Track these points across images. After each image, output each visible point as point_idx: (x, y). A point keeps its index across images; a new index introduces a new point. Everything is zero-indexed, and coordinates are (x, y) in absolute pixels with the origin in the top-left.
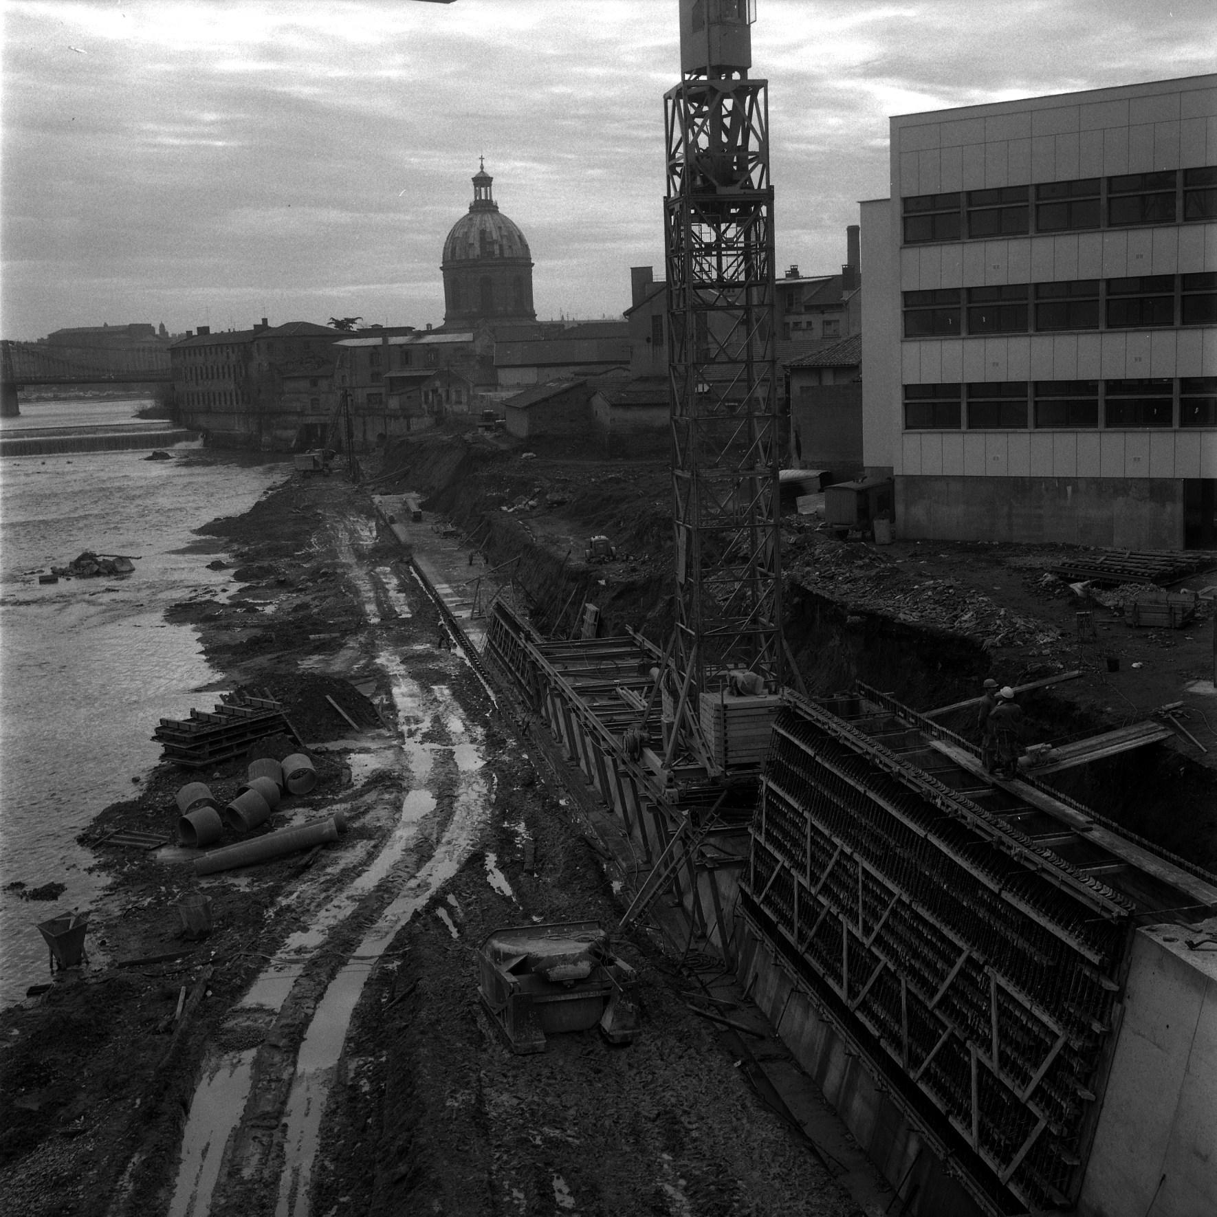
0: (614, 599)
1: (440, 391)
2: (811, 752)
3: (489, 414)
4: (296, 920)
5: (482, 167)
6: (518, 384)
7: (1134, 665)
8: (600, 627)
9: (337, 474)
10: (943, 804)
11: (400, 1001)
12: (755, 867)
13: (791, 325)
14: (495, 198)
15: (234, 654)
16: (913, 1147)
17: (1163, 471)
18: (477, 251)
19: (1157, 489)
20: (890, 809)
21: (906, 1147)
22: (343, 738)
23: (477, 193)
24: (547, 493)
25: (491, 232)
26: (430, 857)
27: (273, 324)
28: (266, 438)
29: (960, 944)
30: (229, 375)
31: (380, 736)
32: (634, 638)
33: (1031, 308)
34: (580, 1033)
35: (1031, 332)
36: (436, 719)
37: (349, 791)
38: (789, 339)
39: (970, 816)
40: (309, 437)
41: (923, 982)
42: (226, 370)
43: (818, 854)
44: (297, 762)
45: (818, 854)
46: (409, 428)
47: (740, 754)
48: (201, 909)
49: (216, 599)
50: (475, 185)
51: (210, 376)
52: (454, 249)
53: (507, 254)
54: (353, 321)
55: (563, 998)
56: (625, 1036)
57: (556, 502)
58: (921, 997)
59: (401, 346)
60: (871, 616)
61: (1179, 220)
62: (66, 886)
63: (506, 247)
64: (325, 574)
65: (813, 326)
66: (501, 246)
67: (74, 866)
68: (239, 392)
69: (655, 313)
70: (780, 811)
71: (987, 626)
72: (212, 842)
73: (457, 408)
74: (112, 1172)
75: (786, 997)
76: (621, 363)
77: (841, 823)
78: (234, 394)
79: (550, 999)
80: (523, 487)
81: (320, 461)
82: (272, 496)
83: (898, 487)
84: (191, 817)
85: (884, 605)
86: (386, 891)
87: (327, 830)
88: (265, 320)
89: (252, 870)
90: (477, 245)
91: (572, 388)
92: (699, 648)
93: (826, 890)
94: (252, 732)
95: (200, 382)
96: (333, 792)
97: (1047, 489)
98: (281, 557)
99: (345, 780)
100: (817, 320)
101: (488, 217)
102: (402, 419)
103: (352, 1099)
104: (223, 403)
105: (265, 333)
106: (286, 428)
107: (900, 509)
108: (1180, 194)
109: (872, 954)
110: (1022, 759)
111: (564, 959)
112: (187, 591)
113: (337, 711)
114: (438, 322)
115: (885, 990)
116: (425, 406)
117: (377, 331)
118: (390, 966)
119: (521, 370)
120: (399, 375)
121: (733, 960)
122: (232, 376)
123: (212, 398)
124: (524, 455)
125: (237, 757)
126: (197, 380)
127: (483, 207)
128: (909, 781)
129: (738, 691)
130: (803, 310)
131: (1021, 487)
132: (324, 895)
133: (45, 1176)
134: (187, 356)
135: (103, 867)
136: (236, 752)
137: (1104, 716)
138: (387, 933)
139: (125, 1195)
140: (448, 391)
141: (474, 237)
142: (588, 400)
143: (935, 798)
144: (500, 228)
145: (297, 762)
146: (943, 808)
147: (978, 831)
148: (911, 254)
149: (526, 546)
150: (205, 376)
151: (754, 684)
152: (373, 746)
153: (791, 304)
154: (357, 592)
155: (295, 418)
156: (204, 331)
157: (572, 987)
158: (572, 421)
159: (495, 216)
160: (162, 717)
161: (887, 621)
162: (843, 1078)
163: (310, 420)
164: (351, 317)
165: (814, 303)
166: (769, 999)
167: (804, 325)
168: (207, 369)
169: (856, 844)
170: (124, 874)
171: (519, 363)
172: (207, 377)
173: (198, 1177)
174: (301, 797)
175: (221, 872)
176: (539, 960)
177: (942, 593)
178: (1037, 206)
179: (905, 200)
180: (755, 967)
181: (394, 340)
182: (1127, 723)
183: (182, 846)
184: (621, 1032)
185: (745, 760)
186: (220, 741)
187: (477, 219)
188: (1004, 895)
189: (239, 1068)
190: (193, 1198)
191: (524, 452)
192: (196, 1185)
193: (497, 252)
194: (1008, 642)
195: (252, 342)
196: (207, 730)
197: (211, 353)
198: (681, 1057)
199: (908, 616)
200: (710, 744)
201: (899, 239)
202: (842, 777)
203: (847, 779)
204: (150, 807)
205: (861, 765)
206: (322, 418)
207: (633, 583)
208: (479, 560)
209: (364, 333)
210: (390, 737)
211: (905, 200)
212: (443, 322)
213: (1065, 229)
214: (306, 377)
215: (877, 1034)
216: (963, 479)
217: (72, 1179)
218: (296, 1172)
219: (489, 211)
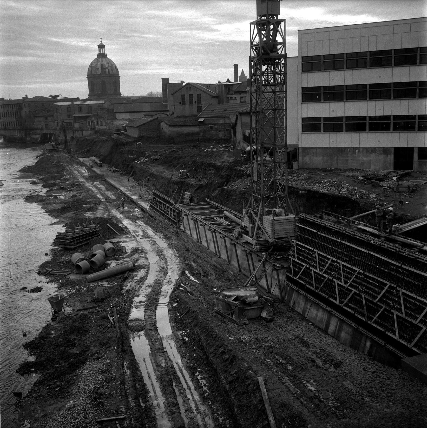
0: (196, 190)
1: (94, 121)
2: (315, 231)
3: (118, 130)
4: (133, 293)
5: (101, 42)
7: (406, 203)
8: (191, 200)
9: (61, 151)
10: (374, 242)
11: (185, 314)
12: (293, 269)
14: (106, 52)
15: (58, 212)
16: (368, 344)
17: (387, 144)
19: (385, 151)
20: (352, 246)
21: (365, 345)
22: (115, 238)
23: (99, 51)
24: (151, 156)
26: (167, 273)
27: (29, 97)
28: (28, 139)
29: (386, 282)
31: (127, 237)
32: (210, 202)
33: (345, 93)
34: (255, 319)
35: (345, 100)
36: (143, 231)
37: (127, 255)
38: (229, 103)
39: (386, 245)
40: (45, 139)
41: (370, 295)
43: (320, 262)
44: (108, 245)
45: (320, 262)
46: (83, 135)
47: (278, 234)
48: (102, 291)
49: (40, 194)
50: (99, 48)
52: (91, 71)
53: (111, 72)
54: (58, 96)
55: (250, 308)
56: (271, 318)
57: (155, 159)
58: (371, 299)
59: (78, 105)
60: (309, 191)
61: (393, 66)
62: (42, 287)
64: (77, 185)
66: (109, 70)
67: (41, 281)
70: (303, 251)
71: (352, 193)
72: (87, 272)
73: (101, 128)
74: (121, 367)
75: (308, 307)
76: (162, 111)
77: (331, 252)
79: (246, 308)
80: (142, 154)
81: (55, 146)
82: (40, 159)
83: (300, 151)
84: (80, 264)
85: (315, 187)
86: (158, 285)
87: (130, 266)
88: (26, 96)
89: (106, 280)
90: (100, 69)
91: (153, 120)
93: (326, 272)
94: (89, 236)
96: (122, 255)
97: (349, 151)
98: (56, 179)
99: (124, 251)
100: (238, 97)
101: (104, 59)
102: (80, 131)
103: (184, 343)
105: (27, 100)
106: (36, 135)
107: (301, 158)
108: (393, 57)
110: (393, 229)
111: (250, 296)
112: (28, 192)
113: (111, 229)
114: (86, 96)
115: (356, 299)
117: (66, 100)
118: (174, 305)
119: (124, 114)
120: (78, 115)
121: (283, 298)
122: (15, 116)
123: (6, 124)
124: (138, 143)
125: (85, 244)
127: (102, 55)
128: (359, 237)
129: (276, 215)
131: (341, 151)
132: (138, 286)
133: (96, 371)
135: (52, 281)
136: (84, 243)
137: (408, 217)
138: (166, 296)
139: (128, 373)
140: (97, 121)
141: (99, 66)
142: (159, 124)
143: (371, 241)
145: (108, 245)
146: (375, 244)
147: (389, 249)
148: (305, 75)
149: (151, 174)
151: (281, 212)
152: (128, 240)
153: (229, 91)
154: (92, 191)
157: (253, 304)
160: (58, 231)
161: (315, 193)
162: (336, 327)
163: (45, 132)
164: (57, 94)
165: (236, 91)
166: (301, 308)
167: (234, 98)
169: (338, 258)
170: (61, 283)
171: (123, 111)
173: (146, 367)
174: (111, 257)
175: (96, 281)
176: (242, 297)
177: (332, 183)
178: (347, 60)
179: (303, 57)
180: (293, 299)
181: (76, 103)
182: (417, 219)
183: (77, 274)
184: (269, 317)
185: (280, 237)
186: (79, 239)
187: (100, 60)
188: (403, 266)
189: (141, 337)
190: (148, 373)
191: (137, 142)
192: (147, 369)
193: (107, 72)
194: (361, 197)
196: (76, 235)
198: (291, 323)
199: (322, 191)
200: (269, 232)
201: (301, 71)
202: (330, 237)
203: (332, 238)
204: (61, 262)
205: (337, 233)
207: (202, 185)
208: (131, 179)
209: (61, 100)
210: (131, 237)
211: (303, 57)
213: (355, 68)
214: (42, 116)
215: (353, 312)
216: (322, 148)
217: (108, 370)
218: (177, 364)
219: (104, 57)
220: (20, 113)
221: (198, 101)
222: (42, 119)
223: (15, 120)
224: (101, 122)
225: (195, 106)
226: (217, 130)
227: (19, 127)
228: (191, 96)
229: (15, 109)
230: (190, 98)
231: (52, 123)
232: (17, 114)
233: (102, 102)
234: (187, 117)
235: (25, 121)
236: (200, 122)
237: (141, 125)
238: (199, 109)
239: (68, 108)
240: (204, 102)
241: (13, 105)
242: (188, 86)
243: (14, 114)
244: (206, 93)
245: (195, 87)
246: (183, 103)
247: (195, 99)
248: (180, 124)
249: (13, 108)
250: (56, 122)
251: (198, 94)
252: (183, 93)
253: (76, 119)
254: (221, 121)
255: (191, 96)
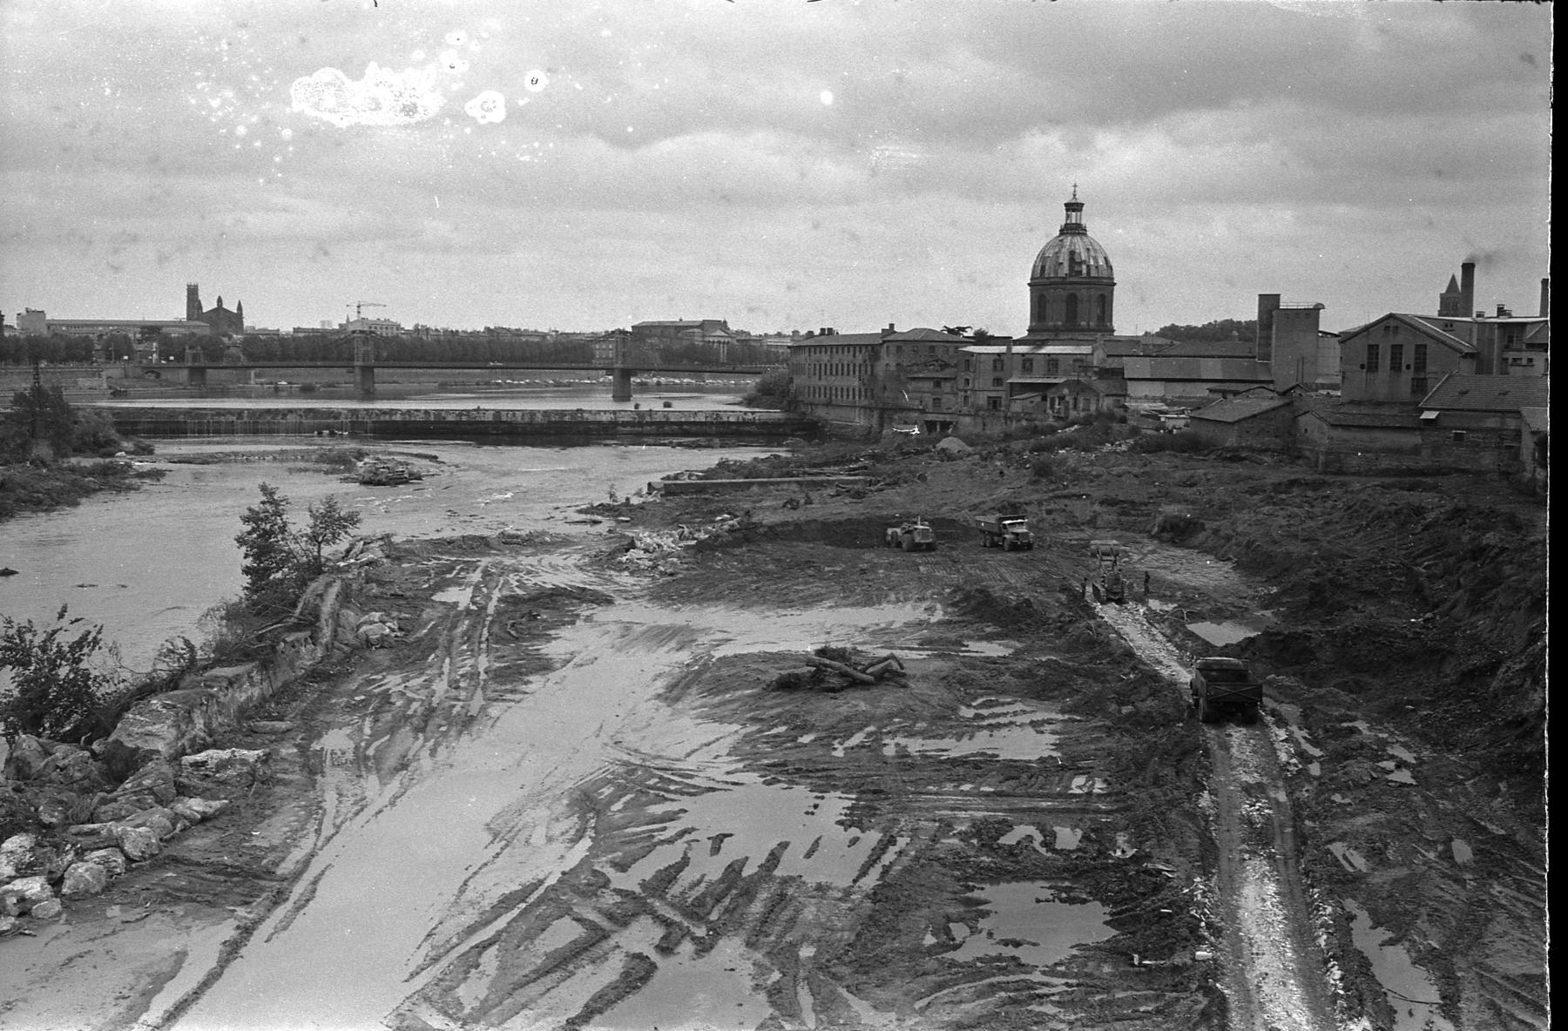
1: (1067, 399)
6: (1146, 396)
13: (1510, 361)
18: (1066, 270)
23: (1068, 217)
25: (1080, 254)
30: (854, 373)
42: (851, 368)
50: (1067, 210)
51: (834, 373)
52: (1043, 268)
53: (1093, 273)
54: (963, 329)
59: (1023, 355)
65: (1534, 363)
66: (1088, 266)
68: (863, 390)
69: (1371, 343)
78: (857, 389)
88: (892, 326)
90: (1066, 264)
92: (815, 740)
95: (823, 377)
101: (1077, 239)
104: (845, 397)
105: (891, 338)
114: (1022, 333)
116: (1049, 411)
126: (820, 375)
130: (1524, 347)
134: (812, 354)
140: (1075, 399)
141: (1064, 258)
144: (1088, 249)
150: (828, 372)
158: (1277, 437)
159: (1085, 239)
167: (1524, 362)
168: (843, 365)
171: (1148, 377)
172: (831, 374)
187: (1068, 240)
193: (1084, 271)
195: (882, 344)
197: (837, 352)
206: (941, 416)
212: (1027, 333)
220: (872, 366)
222: (928, 385)
223: (857, 384)
224: (1087, 400)
225: (1407, 377)
226: (1478, 445)
227: (865, 402)
228: (1397, 350)
229: (860, 358)
231: (951, 397)
233: (1086, 349)
234: (1379, 404)
235: (885, 388)
236: (1428, 421)
237: (1245, 419)
238: (1420, 386)
239: (995, 361)
242: (1392, 323)
243: (857, 368)
244: (1444, 343)
245: (1411, 325)
246: (1371, 366)
247: (1408, 357)
248: (1364, 422)
249: (854, 356)
254: (1492, 423)
255: (1397, 350)
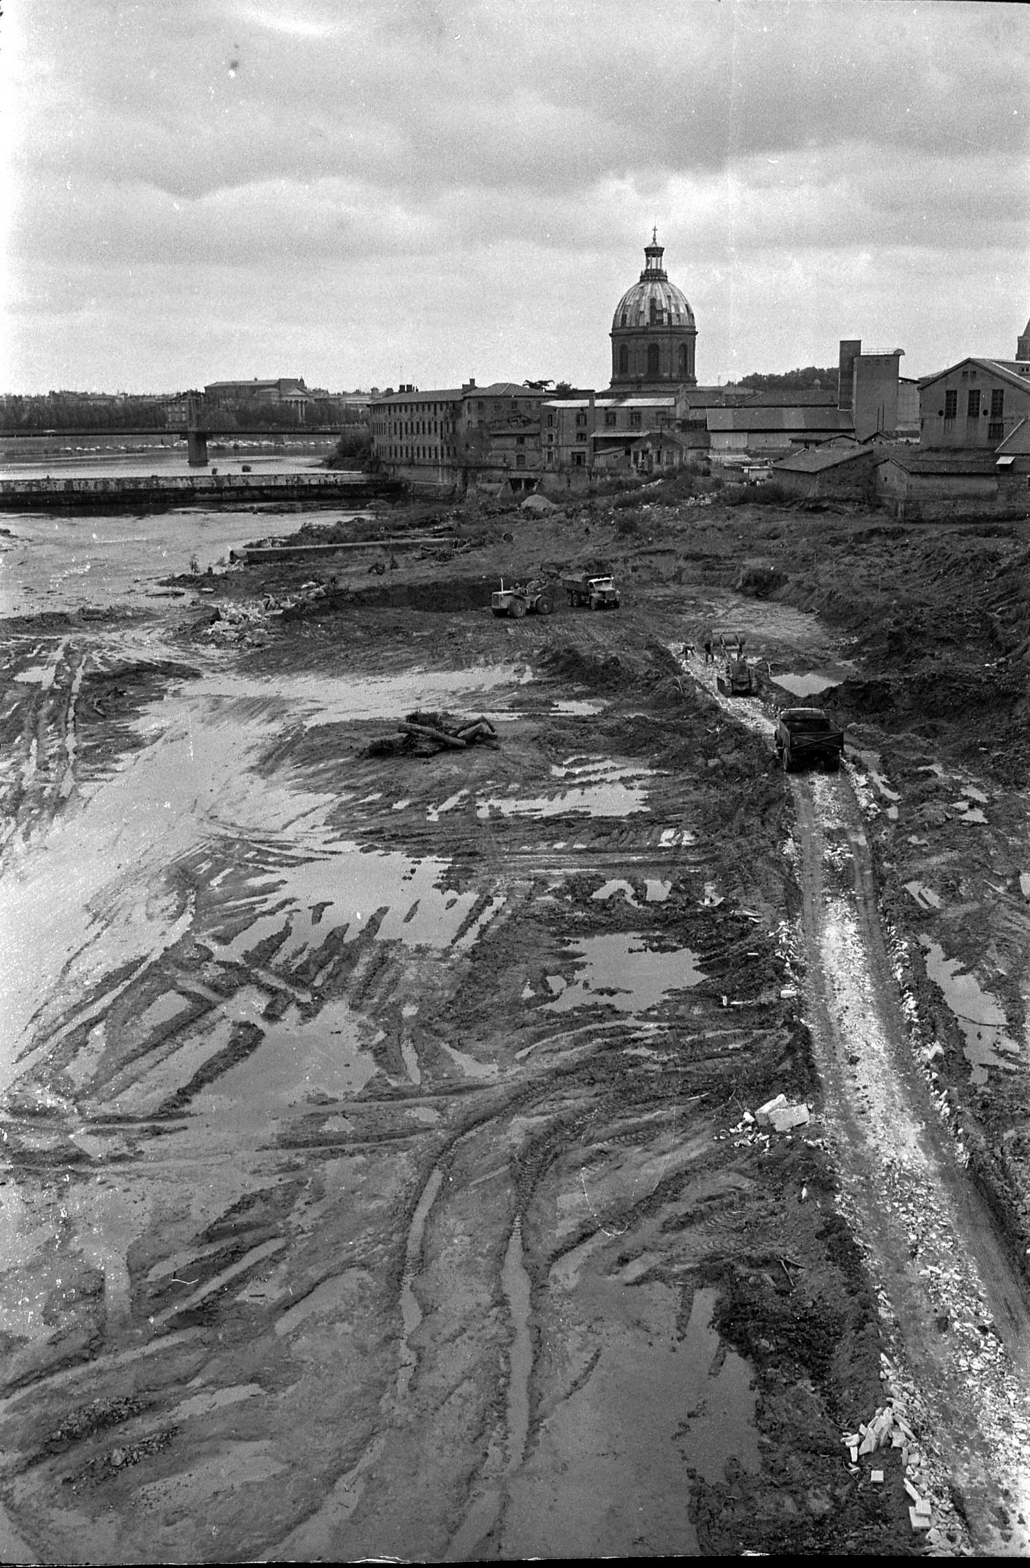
18: (647, 319)
23: (648, 262)
42: (433, 426)
50: (647, 255)
52: (624, 317)
53: (675, 322)
54: (545, 383)
59: (606, 408)
63: (674, 316)
66: (670, 315)
88: (472, 381)
90: (647, 313)
95: (404, 435)
101: (658, 286)
105: (473, 393)
106: (490, 481)
109: (734, 1006)
116: (633, 466)
140: (659, 453)
141: (645, 306)
142: (876, 466)
155: (501, 472)
156: (407, 389)
193: (666, 320)
195: (462, 401)
214: (513, 435)
220: (454, 423)
221: (993, 409)
222: (511, 442)
223: (438, 441)
224: (670, 454)
225: (984, 421)
227: (447, 461)
228: (974, 395)
229: (441, 415)
230: (970, 399)
231: (535, 453)
232: (445, 426)
233: (666, 402)
234: (957, 451)
240: (1013, 413)
241: (435, 403)
242: (970, 368)
243: (439, 426)
244: (1020, 388)
247: (986, 401)
248: (945, 469)
249: (435, 413)
250: (545, 450)
251: (995, 391)
252: (950, 387)
253: (600, 443)
255: (974, 395)
